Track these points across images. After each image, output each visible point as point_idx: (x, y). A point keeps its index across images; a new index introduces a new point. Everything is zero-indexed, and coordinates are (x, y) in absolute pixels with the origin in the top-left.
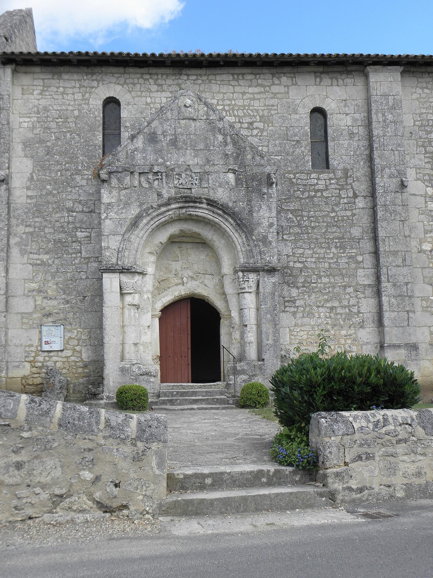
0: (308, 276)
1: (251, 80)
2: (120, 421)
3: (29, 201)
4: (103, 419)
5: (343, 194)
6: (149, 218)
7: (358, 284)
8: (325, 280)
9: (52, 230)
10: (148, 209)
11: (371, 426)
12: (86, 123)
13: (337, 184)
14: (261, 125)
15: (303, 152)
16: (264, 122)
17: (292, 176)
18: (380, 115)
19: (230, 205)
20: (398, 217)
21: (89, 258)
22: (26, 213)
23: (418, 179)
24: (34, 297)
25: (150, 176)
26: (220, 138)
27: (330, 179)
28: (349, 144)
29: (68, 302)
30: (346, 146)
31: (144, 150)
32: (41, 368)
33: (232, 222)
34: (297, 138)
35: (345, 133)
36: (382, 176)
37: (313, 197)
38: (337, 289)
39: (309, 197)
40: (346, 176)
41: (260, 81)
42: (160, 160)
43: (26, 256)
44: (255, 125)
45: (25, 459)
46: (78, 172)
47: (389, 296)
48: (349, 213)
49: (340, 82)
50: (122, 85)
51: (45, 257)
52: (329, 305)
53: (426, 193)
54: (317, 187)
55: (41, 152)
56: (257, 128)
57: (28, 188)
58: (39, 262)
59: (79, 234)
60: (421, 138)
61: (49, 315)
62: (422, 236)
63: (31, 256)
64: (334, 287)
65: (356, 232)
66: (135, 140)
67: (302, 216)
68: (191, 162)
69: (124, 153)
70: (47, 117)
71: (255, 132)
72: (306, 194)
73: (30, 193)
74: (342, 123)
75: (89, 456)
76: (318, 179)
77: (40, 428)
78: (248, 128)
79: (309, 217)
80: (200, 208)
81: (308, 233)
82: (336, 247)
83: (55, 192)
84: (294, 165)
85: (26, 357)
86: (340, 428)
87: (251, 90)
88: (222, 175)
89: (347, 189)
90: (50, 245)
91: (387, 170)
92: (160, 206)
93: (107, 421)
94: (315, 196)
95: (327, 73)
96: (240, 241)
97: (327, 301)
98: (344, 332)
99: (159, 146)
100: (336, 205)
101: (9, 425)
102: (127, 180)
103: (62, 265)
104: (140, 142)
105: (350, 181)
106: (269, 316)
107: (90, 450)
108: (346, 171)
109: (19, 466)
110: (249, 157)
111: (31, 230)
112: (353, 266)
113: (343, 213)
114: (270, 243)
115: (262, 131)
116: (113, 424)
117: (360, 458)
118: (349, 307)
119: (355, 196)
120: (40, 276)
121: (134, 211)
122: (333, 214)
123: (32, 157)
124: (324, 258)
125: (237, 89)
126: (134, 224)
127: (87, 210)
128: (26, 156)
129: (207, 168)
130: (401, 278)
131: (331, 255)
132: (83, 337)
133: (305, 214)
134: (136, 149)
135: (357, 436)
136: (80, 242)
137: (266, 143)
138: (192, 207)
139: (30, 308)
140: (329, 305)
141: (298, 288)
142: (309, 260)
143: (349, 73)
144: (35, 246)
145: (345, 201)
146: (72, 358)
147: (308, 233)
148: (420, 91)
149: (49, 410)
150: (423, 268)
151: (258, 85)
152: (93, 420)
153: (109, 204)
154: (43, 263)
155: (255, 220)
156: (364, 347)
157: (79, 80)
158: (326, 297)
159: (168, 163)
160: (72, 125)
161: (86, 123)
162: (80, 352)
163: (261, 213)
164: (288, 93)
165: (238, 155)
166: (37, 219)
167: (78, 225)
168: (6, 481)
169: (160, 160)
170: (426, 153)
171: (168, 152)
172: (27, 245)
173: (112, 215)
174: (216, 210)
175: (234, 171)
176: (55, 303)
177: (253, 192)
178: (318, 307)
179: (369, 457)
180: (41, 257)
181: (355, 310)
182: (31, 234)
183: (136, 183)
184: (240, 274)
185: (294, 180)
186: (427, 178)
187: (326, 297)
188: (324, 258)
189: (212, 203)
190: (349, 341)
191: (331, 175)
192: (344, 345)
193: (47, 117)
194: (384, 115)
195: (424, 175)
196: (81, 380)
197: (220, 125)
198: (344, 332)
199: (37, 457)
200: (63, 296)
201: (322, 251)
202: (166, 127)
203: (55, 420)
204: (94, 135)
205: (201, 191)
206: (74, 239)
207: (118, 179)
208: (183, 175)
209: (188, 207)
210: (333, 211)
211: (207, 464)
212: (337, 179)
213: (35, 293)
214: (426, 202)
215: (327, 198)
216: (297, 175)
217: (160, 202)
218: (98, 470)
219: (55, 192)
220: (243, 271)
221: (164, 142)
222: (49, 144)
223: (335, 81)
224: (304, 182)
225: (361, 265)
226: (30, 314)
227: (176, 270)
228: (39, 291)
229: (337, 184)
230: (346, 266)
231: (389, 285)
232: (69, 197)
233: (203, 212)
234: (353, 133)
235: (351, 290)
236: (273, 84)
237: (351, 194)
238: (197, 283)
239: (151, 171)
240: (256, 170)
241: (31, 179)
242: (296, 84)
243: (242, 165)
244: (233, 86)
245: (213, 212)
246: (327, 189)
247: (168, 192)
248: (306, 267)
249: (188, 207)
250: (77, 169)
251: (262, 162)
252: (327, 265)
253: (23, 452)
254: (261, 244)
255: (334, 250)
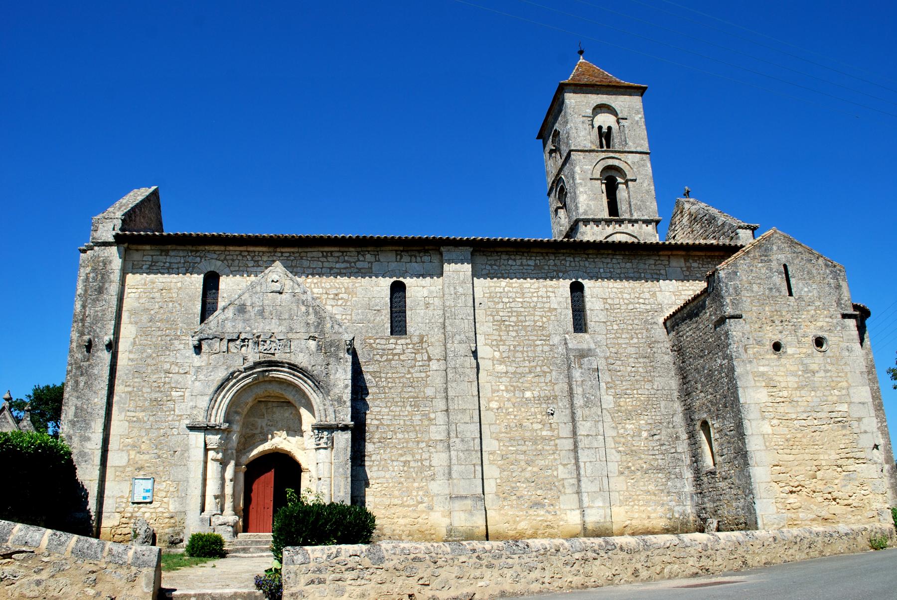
0: (384, 432)
1: (338, 257)
2: (120, 550)
3: (130, 363)
4: (107, 549)
5: (419, 357)
6: (234, 381)
7: (430, 440)
8: (400, 436)
9: (149, 390)
10: (234, 372)
11: (325, 557)
12: (187, 294)
13: (413, 348)
14: (345, 296)
15: (383, 320)
16: (349, 294)
17: (372, 341)
18: (452, 288)
19: (310, 368)
20: (466, 379)
21: (181, 416)
22: (126, 374)
23: (486, 344)
24: (128, 451)
25: (238, 342)
26: (303, 309)
27: (407, 344)
28: (425, 313)
29: (159, 457)
30: (422, 314)
31: (234, 320)
32: (130, 518)
33: (311, 383)
34: (378, 308)
35: (422, 303)
36: (453, 342)
37: (391, 360)
38: (411, 444)
39: (386, 361)
40: (421, 342)
41: (346, 258)
42: (248, 329)
43: (123, 414)
44: (340, 296)
45: (44, 578)
46: (177, 338)
47: (457, 451)
48: (423, 375)
49: (419, 259)
50: (222, 261)
51: (141, 415)
52: (402, 459)
53: (494, 357)
54: (395, 352)
55: (145, 318)
56: (342, 299)
57: (130, 352)
58: (135, 419)
59: (173, 393)
60: (489, 308)
61: (140, 469)
62: (489, 395)
63: (129, 414)
64: (407, 442)
65: (430, 392)
66: (226, 311)
67: (381, 377)
68: (275, 331)
69: (215, 322)
70: (153, 288)
71: (340, 302)
72: (385, 358)
73: (132, 356)
74: (419, 295)
75: (93, 576)
76: (396, 344)
77: (57, 555)
78: (334, 299)
79: (386, 379)
80: (281, 371)
81: (385, 393)
82: (411, 406)
83: (154, 355)
84: (374, 331)
85: (117, 508)
86: (299, 558)
87: (338, 266)
88: (303, 342)
89: (422, 353)
90: (147, 404)
91: (457, 337)
92: (246, 369)
93: (110, 550)
94: (393, 359)
95: (407, 251)
96: (318, 400)
97: (402, 455)
98: (416, 485)
99: (247, 316)
100: (411, 367)
101: (33, 552)
102: (216, 345)
103: (156, 421)
104: (230, 313)
105: (425, 345)
106: (341, 470)
107: (94, 572)
108: (421, 337)
109: (38, 583)
110: (329, 325)
111: (130, 389)
112: (426, 423)
113: (418, 375)
114: (345, 402)
115: (346, 301)
116: (114, 552)
117: (313, 582)
118: (422, 460)
119: (430, 359)
120: (135, 433)
121: (222, 374)
122: (409, 376)
123: (136, 323)
124: (400, 415)
125: (326, 264)
126: (221, 387)
127: (183, 372)
128: (131, 323)
129: (290, 336)
130: (468, 434)
131: (406, 413)
132: (172, 489)
133: (383, 375)
134: (227, 319)
135: (312, 564)
136: (174, 401)
137: (349, 312)
138: (275, 370)
139: (124, 462)
140: (402, 459)
141: (374, 443)
142: (385, 417)
143: (426, 251)
144: (132, 404)
145: (420, 363)
146: (160, 509)
147: (385, 393)
148: (488, 267)
149: (66, 541)
150: (490, 425)
151: (345, 261)
152: (99, 549)
153: (199, 367)
154: (139, 420)
155: (332, 382)
156: (435, 498)
157: (184, 257)
158: (400, 452)
159: (255, 331)
160: (175, 295)
161: (187, 294)
162: (168, 503)
163: (338, 375)
164: (371, 268)
165: (319, 324)
166: (136, 380)
167: (173, 385)
168: (28, 595)
169: (248, 329)
170: (494, 321)
171: (255, 320)
172: (125, 404)
173: (201, 377)
174: (296, 373)
175: (314, 338)
176: (146, 457)
177: (330, 357)
178: (393, 461)
179: (321, 582)
180: (137, 414)
181: (427, 463)
182: (130, 393)
183: (225, 349)
184: (316, 431)
185: (374, 345)
186: (494, 343)
187: (400, 452)
188: (400, 415)
189: (293, 367)
190: (421, 493)
191: (408, 341)
192: (416, 496)
193: (153, 288)
194: (455, 288)
195: (492, 341)
196: (167, 530)
197: (304, 297)
198: (416, 485)
199: (53, 576)
200: (155, 451)
201: (398, 409)
202: (255, 299)
203: (70, 549)
204: (194, 304)
205: (283, 356)
206: (169, 398)
207: (209, 345)
208: (268, 342)
209: (271, 371)
210: (409, 372)
211: (208, 588)
212: (414, 344)
213: (129, 448)
214: (494, 365)
215: (403, 361)
216: (377, 341)
217: (246, 366)
218: (99, 587)
219: (154, 355)
220: (318, 429)
221: (252, 312)
222: (152, 312)
223: (413, 259)
224: (383, 347)
225: (434, 422)
226: (125, 467)
227: (262, 427)
228: (134, 446)
229: (413, 348)
230: (420, 423)
231: (457, 440)
232: (167, 360)
233: (283, 374)
234: (428, 304)
235: (423, 445)
236: (359, 260)
237: (426, 358)
238: (281, 439)
239: (238, 337)
240: (334, 337)
241: (134, 343)
242: (379, 261)
243: (322, 332)
244: (322, 262)
245: (294, 375)
246: (404, 353)
247: (253, 356)
248: (383, 424)
249: (271, 371)
250: (176, 335)
251: (341, 330)
252: (402, 422)
253: (43, 572)
254: (336, 403)
255: (409, 408)
